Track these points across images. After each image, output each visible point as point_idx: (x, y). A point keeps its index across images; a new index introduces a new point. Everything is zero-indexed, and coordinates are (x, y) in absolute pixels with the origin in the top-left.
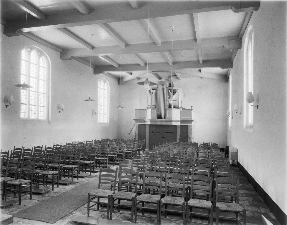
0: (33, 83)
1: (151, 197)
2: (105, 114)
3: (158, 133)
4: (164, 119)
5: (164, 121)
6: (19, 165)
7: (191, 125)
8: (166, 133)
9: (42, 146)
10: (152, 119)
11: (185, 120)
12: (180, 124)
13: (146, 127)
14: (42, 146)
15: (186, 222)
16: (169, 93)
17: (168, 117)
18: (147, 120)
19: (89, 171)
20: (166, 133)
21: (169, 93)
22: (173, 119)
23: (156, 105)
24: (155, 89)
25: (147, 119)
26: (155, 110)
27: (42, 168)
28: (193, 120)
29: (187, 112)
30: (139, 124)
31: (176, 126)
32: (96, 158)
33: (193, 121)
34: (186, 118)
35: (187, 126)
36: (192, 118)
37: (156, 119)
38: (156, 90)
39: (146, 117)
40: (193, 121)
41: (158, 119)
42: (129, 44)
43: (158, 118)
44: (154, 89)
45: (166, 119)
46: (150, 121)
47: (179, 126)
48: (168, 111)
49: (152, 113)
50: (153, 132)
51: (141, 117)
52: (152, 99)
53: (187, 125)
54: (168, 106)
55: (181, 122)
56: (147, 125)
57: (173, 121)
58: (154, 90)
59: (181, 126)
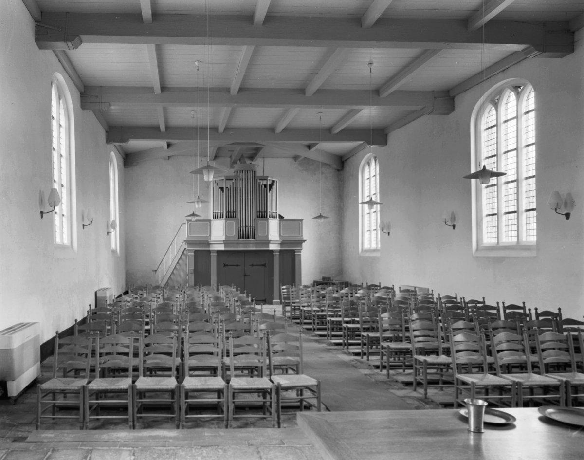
0: (508, 164)
1: (529, 378)
2: (368, 231)
3: (254, 264)
4: (253, 240)
5: (252, 242)
6: (494, 352)
7: (301, 249)
8: (237, 265)
9: (484, 300)
10: (227, 240)
11: (232, 241)
12: (280, 249)
13: (210, 255)
14: (484, 300)
15: (331, 439)
16: (263, 190)
17: (260, 233)
18: (213, 241)
19: (159, 371)
20: (237, 265)
21: (263, 190)
22: (270, 239)
23: (234, 211)
24: (232, 180)
25: (213, 239)
26: (233, 222)
27: (256, 373)
28: (304, 239)
29: (291, 225)
30: (196, 251)
31: (272, 251)
32: (344, 325)
33: (306, 241)
34: (292, 236)
35: (294, 251)
36: (302, 236)
37: (236, 238)
38: (234, 181)
39: (210, 235)
40: (306, 241)
41: (241, 238)
42: (168, 88)
43: (240, 237)
44: (231, 178)
45: (258, 238)
46: (224, 243)
47: (191, 252)
48: (260, 222)
49: (227, 228)
50: (225, 265)
51: (199, 235)
52: (226, 199)
53: (294, 250)
54: (258, 214)
55: (282, 244)
56: (213, 252)
57: (271, 242)
58: (231, 182)
59: (280, 251)
